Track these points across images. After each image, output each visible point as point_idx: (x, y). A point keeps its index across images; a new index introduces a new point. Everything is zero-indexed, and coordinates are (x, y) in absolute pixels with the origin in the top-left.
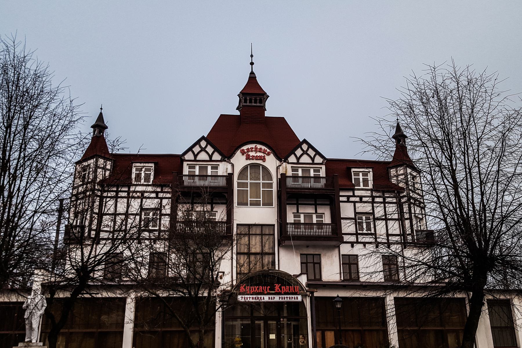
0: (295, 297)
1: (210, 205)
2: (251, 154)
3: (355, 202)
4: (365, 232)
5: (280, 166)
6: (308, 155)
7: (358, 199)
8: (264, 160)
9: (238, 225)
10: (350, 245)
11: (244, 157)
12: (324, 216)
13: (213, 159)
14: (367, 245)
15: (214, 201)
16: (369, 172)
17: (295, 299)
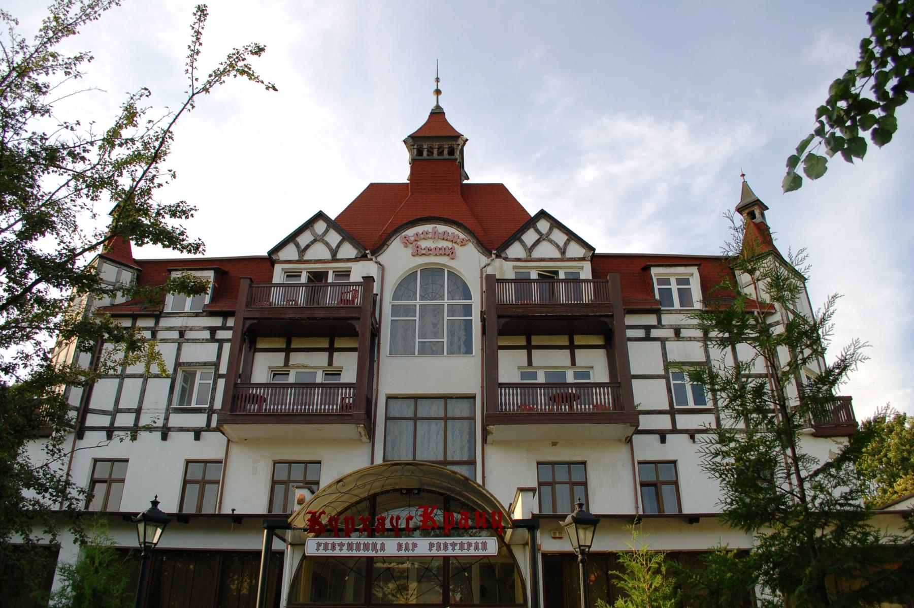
0: (477, 543)
2: (424, 244)
3: (663, 341)
4: (691, 405)
5: (488, 265)
6: (551, 241)
7: (670, 333)
8: (451, 254)
9: (389, 398)
10: (657, 437)
11: (409, 251)
12: (593, 372)
13: (339, 256)
14: (697, 436)
15: (337, 345)
17: (477, 548)
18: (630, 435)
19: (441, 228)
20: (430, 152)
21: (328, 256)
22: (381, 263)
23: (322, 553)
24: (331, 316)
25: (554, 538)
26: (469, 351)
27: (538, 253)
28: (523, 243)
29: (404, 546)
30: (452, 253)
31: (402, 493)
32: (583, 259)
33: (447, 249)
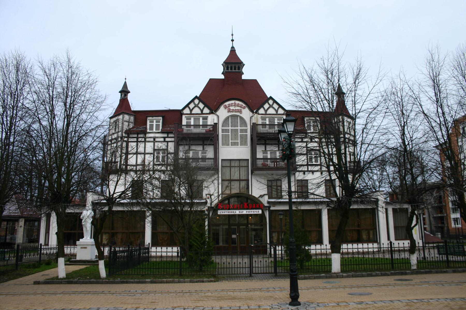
15: (205, 143)
19: (237, 102)
28: (264, 108)
32: (283, 114)
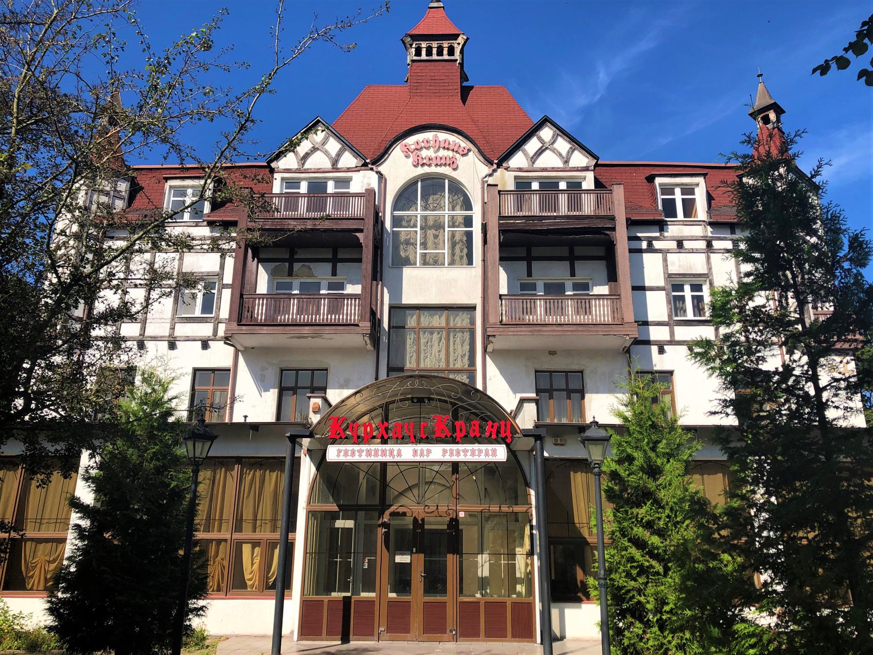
1: (331, 264)
3: (664, 252)
4: (690, 316)
6: (554, 151)
7: (673, 245)
15: (340, 256)
16: (697, 185)
18: (628, 345)
19: (443, 136)
20: (429, 52)
21: (328, 165)
22: (382, 172)
23: (342, 458)
24: (335, 227)
25: (556, 445)
26: (470, 262)
27: (541, 162)
28: (526, 154)
29: (419, 452)
30: (453, 162)
31: (413, 402)
32: (586, 169)
33: (448, 159)
